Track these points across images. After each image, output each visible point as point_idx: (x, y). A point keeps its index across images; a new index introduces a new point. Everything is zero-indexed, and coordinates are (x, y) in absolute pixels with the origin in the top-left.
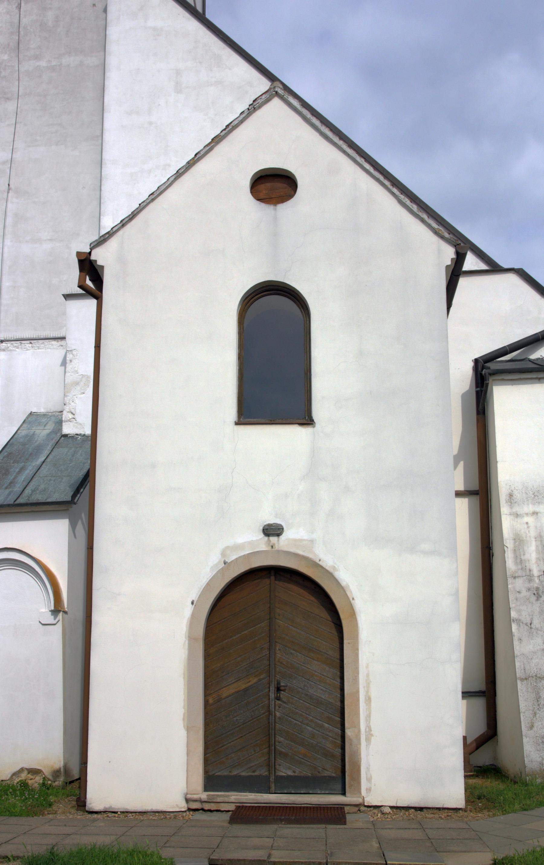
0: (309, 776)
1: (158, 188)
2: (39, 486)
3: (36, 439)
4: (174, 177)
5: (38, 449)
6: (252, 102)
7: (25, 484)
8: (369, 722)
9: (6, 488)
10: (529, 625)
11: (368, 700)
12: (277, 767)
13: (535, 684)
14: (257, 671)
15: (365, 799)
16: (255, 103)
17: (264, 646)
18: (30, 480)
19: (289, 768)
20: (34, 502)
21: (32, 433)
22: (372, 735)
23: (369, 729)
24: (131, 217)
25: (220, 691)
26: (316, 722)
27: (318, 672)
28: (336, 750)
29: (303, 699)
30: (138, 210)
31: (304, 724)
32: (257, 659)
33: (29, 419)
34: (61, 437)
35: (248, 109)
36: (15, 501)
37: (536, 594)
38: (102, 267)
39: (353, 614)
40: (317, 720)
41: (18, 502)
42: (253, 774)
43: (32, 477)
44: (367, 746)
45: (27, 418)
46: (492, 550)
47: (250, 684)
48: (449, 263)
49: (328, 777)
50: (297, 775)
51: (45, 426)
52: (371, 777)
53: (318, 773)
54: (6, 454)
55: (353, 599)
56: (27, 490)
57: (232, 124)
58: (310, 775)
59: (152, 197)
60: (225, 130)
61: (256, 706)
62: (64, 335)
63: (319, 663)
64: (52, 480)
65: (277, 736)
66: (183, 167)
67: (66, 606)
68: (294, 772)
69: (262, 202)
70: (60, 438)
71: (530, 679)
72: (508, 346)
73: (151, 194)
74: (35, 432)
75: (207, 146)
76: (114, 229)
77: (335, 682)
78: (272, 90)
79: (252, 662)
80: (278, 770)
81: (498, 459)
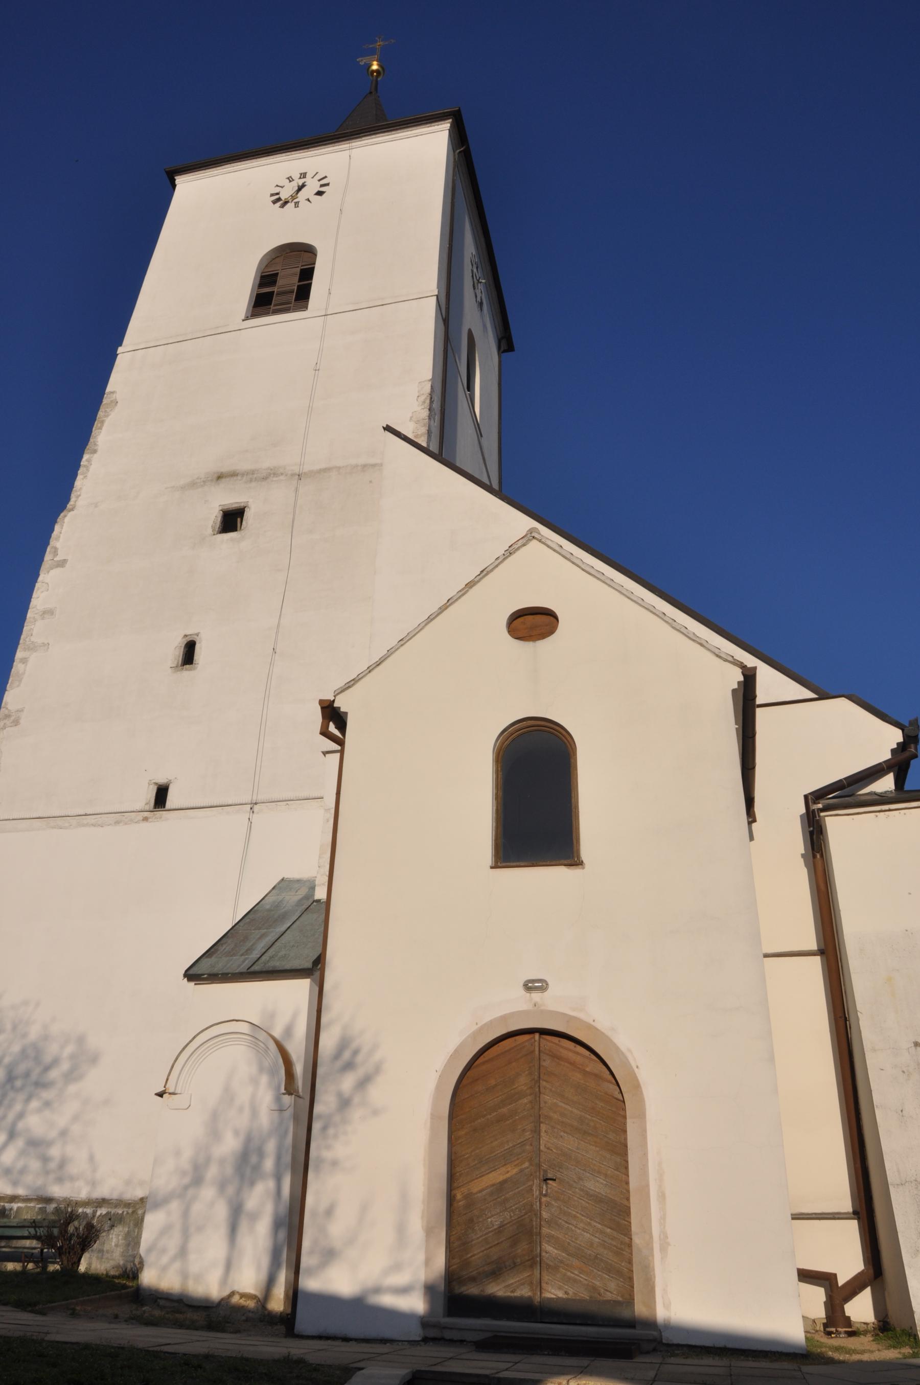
0: (587, 1299)
1: (408, 634)
2: (279, 952)
3: (284, 905)
4: (425, 623)
5: (284, 916)
6: (507, 548)
7: (264, 950)
8: (664, 1227)
9: (242, 955)
10: (900, 1112)
11: (662, 1197)
12: (544, 1285)
13: (915, 1192)
14: (518, 1159)
15: (663, 1334)
16: (511, 549)
17: (526, 1127)
18: (269, 946)
19: (560, 1288)
20: (271, 969)
21: (280, 899)
22: (669, 1244)
23: (664, 1236)
24: (378, 663)
25: (470, 1184)
26: (595, 1226)
27: (596, 1161)
28: (623, 1264)
29: (578, 1196)
30: (386, 657)
31: (579, 1229)
32: (518, 1144)
33: (280, 885)
34: (313, 902)
35: (504, 555)
36: (248, 969)
37: (905, 1071)
38: (346, 713)
39: (637, 1087)
40: (595, 1224)
41: (252, 969)
42: (512, 1295)
43: (272, 943)
44: (662, 1258)
45: (279, 883)
46: (849, 1021)
47: (508, 1175)
48: (736, 686)
49: (612, 1302)
50: (570, 1297)
51: (297, 892)
52: (670, 1303)
53: (599, 1296)
54: (248, 920)
55: (637, 1067)
56: (265, 957)
57: (486, 570)
58: (588, 1298)
59: (402, 643)
60: (479, 575)
61: (517, 1204)
62: (322, 795)
63: (597, 1149)
64: (295, 946)
65: (544, 1244)
66: (435, 612)
67: (300, 1090)
68: (566, 1293)
69: (521, 640)
70: (312, 904)
71: (907, 1184)
72: (845, 779)
73: (401, 640)
74: (284, 897)
75: (460, 591)
76: (360, 676)
77: (618, 1173)
78: (529, 535)
79: (512, 1147)
80: (545, 1290)
81: (841, 908)
